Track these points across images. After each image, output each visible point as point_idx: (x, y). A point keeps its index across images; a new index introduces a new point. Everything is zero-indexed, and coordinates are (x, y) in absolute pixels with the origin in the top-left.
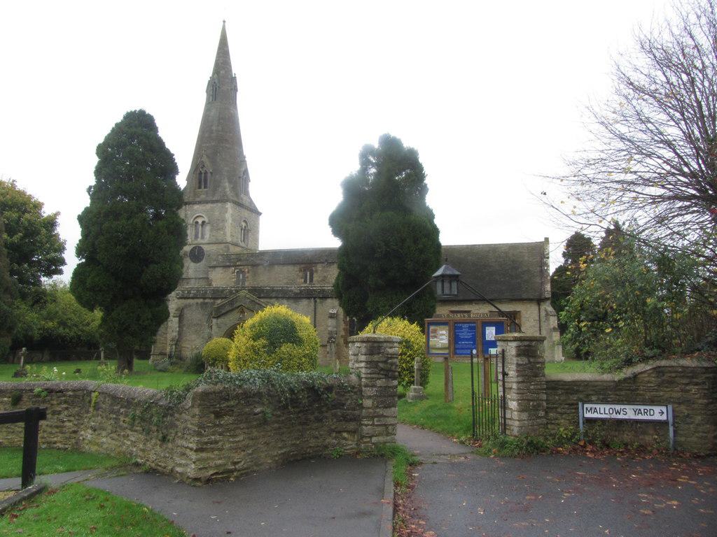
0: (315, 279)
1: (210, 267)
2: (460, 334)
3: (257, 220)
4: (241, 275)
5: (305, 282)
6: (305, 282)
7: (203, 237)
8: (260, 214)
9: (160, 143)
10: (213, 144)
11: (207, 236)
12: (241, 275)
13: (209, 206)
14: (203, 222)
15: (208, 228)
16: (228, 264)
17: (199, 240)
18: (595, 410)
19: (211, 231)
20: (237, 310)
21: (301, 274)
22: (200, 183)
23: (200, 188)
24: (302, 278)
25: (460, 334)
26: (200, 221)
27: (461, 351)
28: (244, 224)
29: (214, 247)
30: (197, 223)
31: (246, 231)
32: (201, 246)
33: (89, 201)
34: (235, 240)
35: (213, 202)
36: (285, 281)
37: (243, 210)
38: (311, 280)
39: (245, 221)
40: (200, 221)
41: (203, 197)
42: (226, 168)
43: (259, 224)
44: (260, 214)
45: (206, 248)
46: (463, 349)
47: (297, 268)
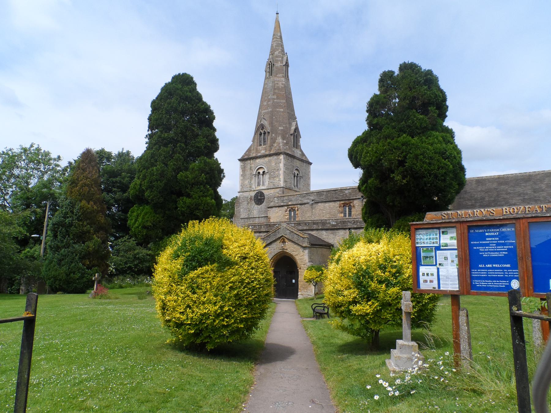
0: (352, 213)
1: (269, 208)
2: (481, 249)
3: (309, 168)
4: (292, 213)
5: (345, 216)
6: (345, 216)
7: (263, 185)
8: (311, 164)
9: (199, 97)
10: (270, 110)
11: (267, 183)
12: (292, 213)
13: (267, 159)
14: (264, 172)
15: (267, 177)
16: (282, 204)
17: (261, 187)
18: (490, 232)
19: (270, 178)
20: (279, 241)
21: (341, 209)
22: (260, 141)
23: (261, 145)
24: (341, 213)
25: (481, 249)
26: (261, 171)
27: (483, 283)
28: (296, 172)
29: (272, 191)
30: (259, 173)
31: (298, 178)
32: (263, 191)
33: (140, 155)
34: (288, 185)
35: (270, 155)
36: (328, 216)
37: (295, 160)
38: (350, 214)
39: (297, 169)
40: (261, 171)
41: (263, 152)
42: (280, 128)
43: (309, 172)
44: (311, 164)
45: (266, 193)
46: (487, 278)
47: (337, 204)
